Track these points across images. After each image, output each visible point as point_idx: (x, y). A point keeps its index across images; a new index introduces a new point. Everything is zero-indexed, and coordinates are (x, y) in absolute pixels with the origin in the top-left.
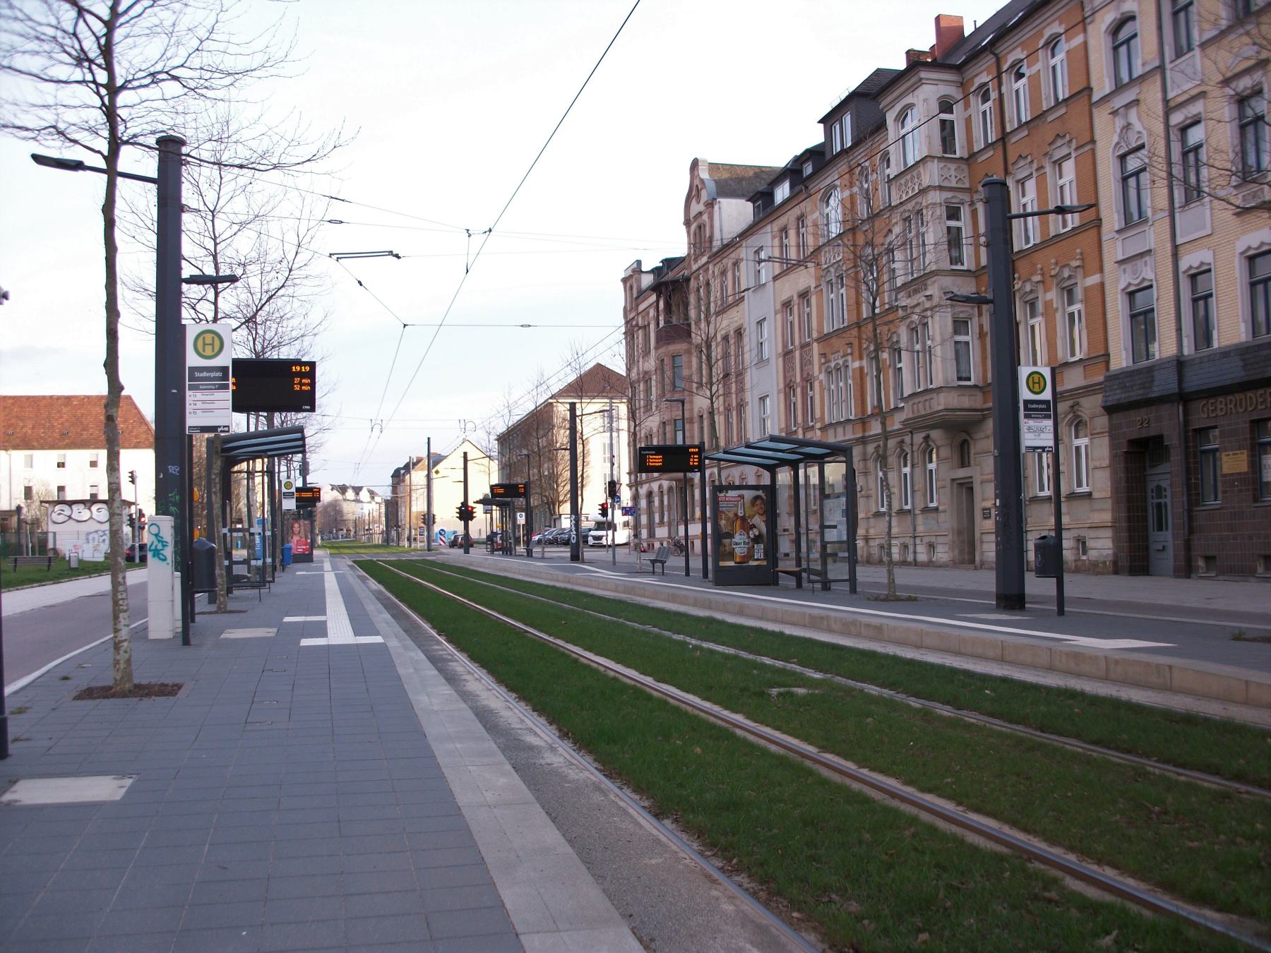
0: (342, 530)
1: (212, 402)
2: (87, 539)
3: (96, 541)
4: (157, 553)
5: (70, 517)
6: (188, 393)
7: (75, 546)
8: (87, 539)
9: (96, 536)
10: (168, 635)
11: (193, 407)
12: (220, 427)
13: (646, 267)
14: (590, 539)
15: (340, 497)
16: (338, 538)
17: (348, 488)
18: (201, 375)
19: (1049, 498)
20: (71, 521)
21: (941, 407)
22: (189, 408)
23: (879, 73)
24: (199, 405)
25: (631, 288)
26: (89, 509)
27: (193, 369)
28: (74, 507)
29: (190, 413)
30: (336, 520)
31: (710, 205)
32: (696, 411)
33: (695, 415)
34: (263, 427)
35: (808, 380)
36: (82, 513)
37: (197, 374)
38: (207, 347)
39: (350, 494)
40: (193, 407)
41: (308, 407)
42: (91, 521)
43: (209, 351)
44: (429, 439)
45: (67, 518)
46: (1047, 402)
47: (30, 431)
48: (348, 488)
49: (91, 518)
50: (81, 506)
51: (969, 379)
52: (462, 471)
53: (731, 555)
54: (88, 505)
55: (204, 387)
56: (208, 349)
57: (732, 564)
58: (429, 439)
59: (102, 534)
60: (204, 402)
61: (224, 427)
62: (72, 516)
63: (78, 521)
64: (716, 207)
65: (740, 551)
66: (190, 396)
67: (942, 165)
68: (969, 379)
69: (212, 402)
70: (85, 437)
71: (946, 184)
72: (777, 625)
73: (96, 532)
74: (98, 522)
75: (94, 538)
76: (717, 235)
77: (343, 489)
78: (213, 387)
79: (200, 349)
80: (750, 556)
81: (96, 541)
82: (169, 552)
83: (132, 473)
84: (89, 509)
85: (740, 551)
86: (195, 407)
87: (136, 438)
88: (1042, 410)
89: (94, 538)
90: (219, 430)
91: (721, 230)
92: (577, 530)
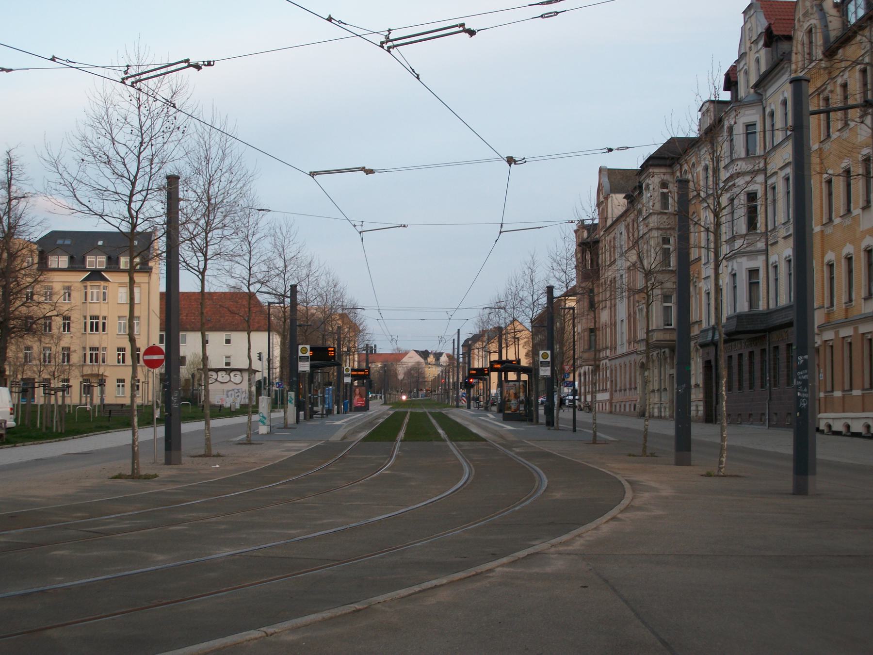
0: (421, 390)
2: (227, 395)
3: (233, 396)
4: (290, 402)
5: (216, 380)
7: (221, 399)
8: (227, 395)
9: (233, 392)
10: (293, 423)
14: (567, 401)
15: (422, 360)
16: (418, 396)
17: (430, 353)
20: (217, 382)
21: (654, 340)
22: (299, 366)
23: (672, 141)
25: (579, 236)
26: (229, 375)
27: (300, 357)
28: (220, 373)
30: (417, 381)
31: (606, 198)
32: (601, 323)
33: (601, 326)
35: (635, 313)
36: (236, 378)
39: (431, 359)
42: (230, 383)
44: (459, 330)
45: (214, 381)
46: (549, 362)
47: (185, 318)
48: (430, 353)
49: (230, 380)
50: (224, 373)
51: (671, 325)
53: (510, 408)
54: (228, 372)
57: (510, 412)
58: (459, 330)
59: (237, 391)
62: (218, 379)
63: (222, 383)
64: (610, 200)
65: (513, 407)
66: (300, 363)
67: (660, 216)
68: (671, 325)
70: (222, 322)
71: (662, 227)
73: (233, 390)
74: (235, 383)
75: (232, 394)
76: (610, 215)
77: (425, 354)
80: (518, 409)
81: (233, 396)
82: (293, 401)
83: (260, 354)
84: (229, 375)
85: (513, 407)
87: (258, 323)
89: (232, 394)
91: (612, 214)
92: (501, 396)
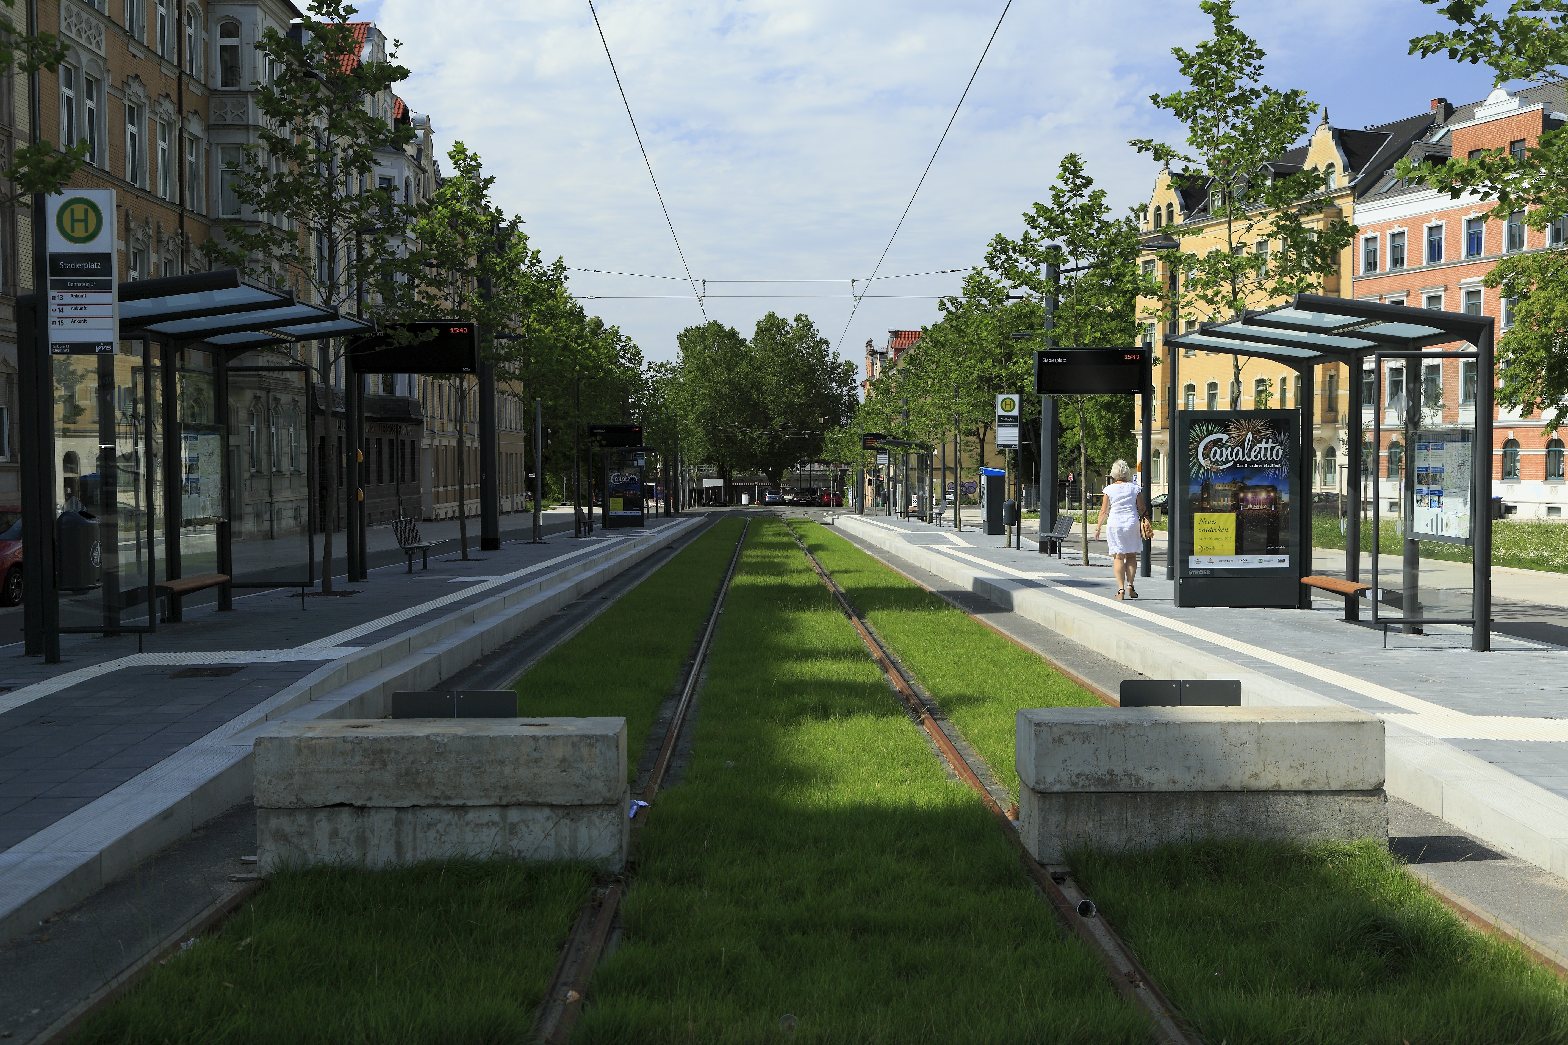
1: (85, 306)
6: (52, 293)
11: (58, 314)
12: (99, 344)
13: (1153, 144)
18: (70, 266)
19: (1464, 435)
24: (68, 312)
29: (54, 323)
34: (401, 379)
37: (63, 265)
38: (76, 224)
40: (58, 314)
41: (469, 369)
43: (1008, 408)
52: (1380, 496)
55: (74, 284)
56: (1008, 407)
60: (74, 306)
61: (105, 344)
69: (85, 306)
72: (823, 675)
78: (88, 285)
79: (68, 228)
86: (61, 314)
88: (1011, 422)
90: (98, 349)
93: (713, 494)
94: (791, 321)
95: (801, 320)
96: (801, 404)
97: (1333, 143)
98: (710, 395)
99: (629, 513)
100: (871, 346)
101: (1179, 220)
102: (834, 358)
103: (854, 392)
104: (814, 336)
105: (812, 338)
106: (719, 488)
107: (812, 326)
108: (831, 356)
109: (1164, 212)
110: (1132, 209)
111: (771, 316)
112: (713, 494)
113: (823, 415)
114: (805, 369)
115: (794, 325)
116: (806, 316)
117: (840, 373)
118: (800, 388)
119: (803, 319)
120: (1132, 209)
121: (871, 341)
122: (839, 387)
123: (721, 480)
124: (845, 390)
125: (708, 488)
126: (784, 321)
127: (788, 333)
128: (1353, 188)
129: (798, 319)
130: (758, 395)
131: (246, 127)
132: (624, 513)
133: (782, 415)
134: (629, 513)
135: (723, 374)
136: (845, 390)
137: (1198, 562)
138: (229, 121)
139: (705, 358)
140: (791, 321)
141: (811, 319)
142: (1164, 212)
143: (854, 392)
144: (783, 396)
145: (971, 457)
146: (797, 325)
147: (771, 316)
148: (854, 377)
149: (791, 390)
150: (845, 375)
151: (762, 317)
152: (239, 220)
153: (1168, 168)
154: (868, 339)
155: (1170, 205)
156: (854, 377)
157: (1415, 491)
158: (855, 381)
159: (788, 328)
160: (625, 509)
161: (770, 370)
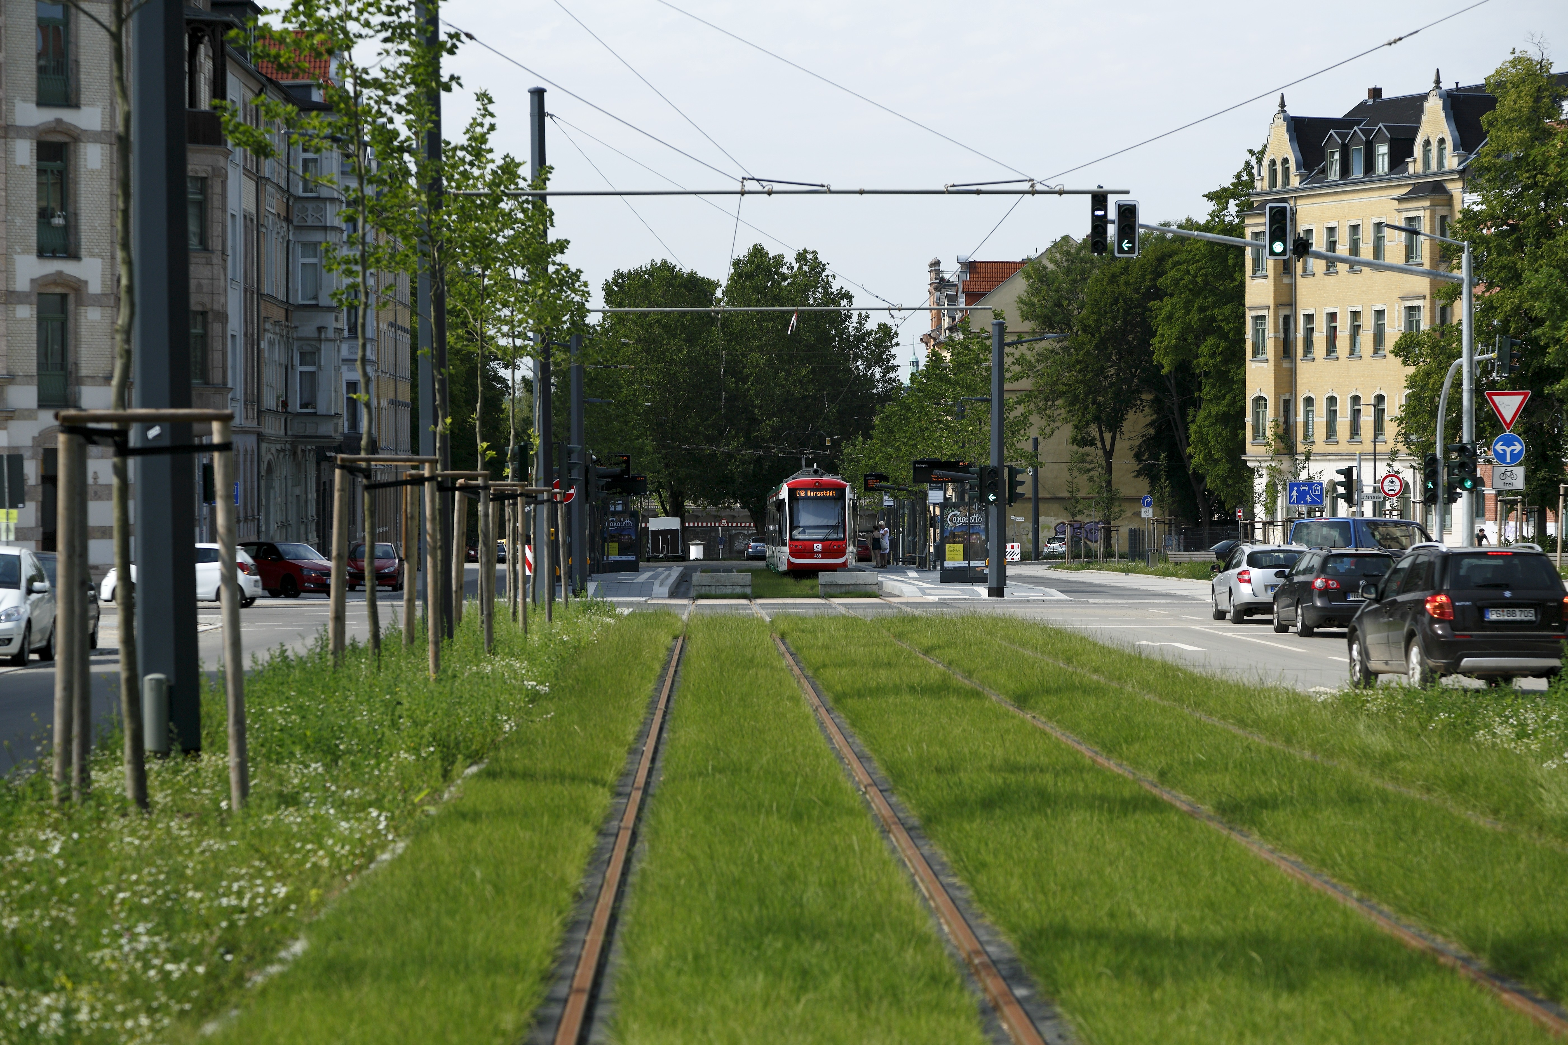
93: (665, 541)
94: (790, 258)
95: (806, 260)
96: (804, 398)
97: (1443, 114)
98: (659, 383)
99: (624, 558)
100: (938, 272)
101: (1295, 181)
102: (859, 322)
103: (892, 375)
104: (826, 285)
105: (825, 288)
106: (673, 532)
107: (824, 270)
108: (855, 318)
109: (1279, 168)
110: (1251, 152)
111: (758, 252)
112: (665, 541)
113: (830, 435)
114: (812, 340)
115: (796, 266)
116: (815, 252)
117: (869, 343)
118: (804, 372)
119: (810, 256)
120: (1251, 152)
121: (937, 263)
122: (868, 367)
123: (678, 519)
124: (878, 372)
125: (656, 533)
126: (779, 261)
127: (784, 278)
128: (1462, 173)
129: (801, 257)
130: (736, 383)
131: (325, 228)
132: (618, 558)
133: (774, 415)
134: (624, 558)
135: (680, 350)
136: (878, 372)
137: (948, 564)
138: (309, 223)
139: (650, 325)
140: (790, 258)
141: (822, 258)
142: (1279, 168)
143: (892, 375)
144: (777, 385)
145: (1091, 479)
146: (800, 268)
147: (758, 252)
148: (893, 351)
149: (788, 373)
150: (877, 347)
151: (742, 252)
152: (317, 306)
153: (1284, 111)
154: (931, 259)
155: (1285, 161)
156: (893, 351)
157: (116, 533)
158: (894, 357)
159: (785, 270)
160: (620, 554)
161: (756, 343)
